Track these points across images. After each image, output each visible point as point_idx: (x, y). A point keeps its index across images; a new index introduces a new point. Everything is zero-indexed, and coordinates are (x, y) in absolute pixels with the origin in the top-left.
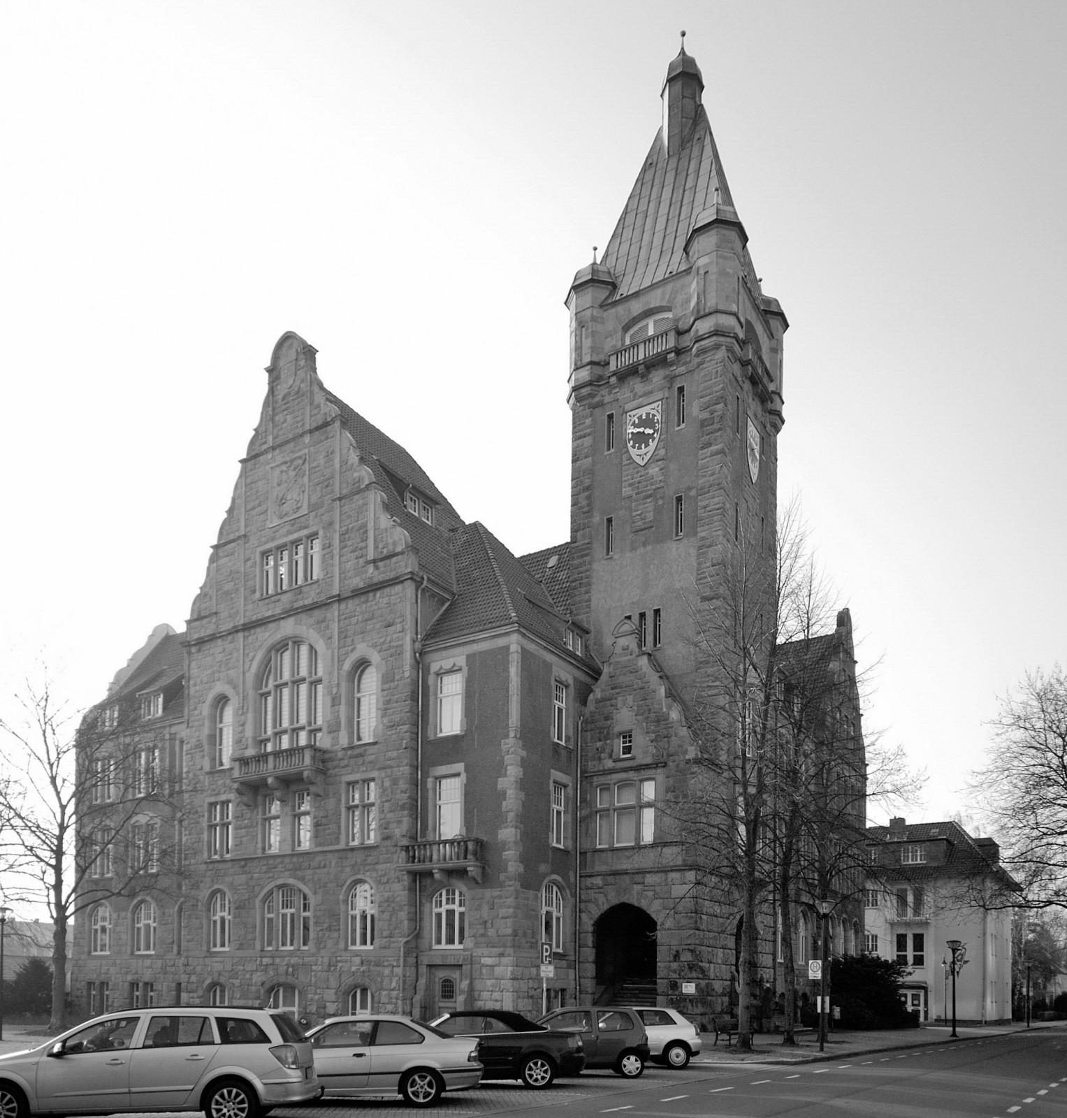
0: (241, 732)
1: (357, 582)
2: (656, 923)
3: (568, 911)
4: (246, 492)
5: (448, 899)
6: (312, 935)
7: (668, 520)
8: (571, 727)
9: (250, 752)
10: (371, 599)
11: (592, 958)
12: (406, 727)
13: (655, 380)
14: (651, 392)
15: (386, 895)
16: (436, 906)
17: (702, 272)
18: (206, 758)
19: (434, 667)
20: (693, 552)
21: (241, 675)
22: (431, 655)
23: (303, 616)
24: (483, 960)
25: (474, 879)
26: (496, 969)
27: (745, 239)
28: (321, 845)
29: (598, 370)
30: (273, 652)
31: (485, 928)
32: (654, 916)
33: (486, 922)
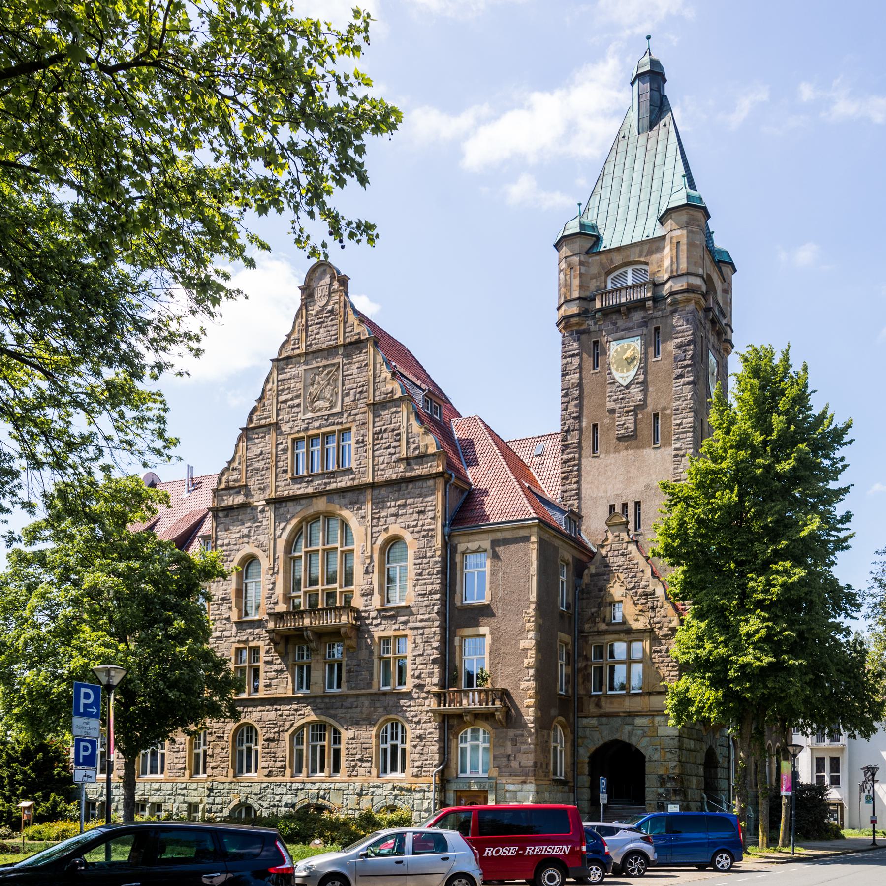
0: (273, 589)
1: (391, 474)
2: (644, 757)
3: (569, 745)
4: (278, 386)
5: (472, 737)
6: (343, 764)
7: (646, 431)
8: (571, 595)
9: (282, 608)
10: (404, 488)
11: (587, 784)
12: (437, 596)
13: (634, 319)
14: (632, 328)
15: (418, 732)
16: (462, 742)
17: (675, 241)
18: (234, 609)
19: (461, 547)
20: (670, 459)
21: (272, 542)
22: (458, 538)
23: (336, 496)
24: (507, 787)
25: (500, 721)
26: (519, 794)
27: (708, 216)
28: (352, 689)
29: (585, 304)
30: (304, 523)
31: (509, 760)
32: (642, 751)
33: (509, 755)
